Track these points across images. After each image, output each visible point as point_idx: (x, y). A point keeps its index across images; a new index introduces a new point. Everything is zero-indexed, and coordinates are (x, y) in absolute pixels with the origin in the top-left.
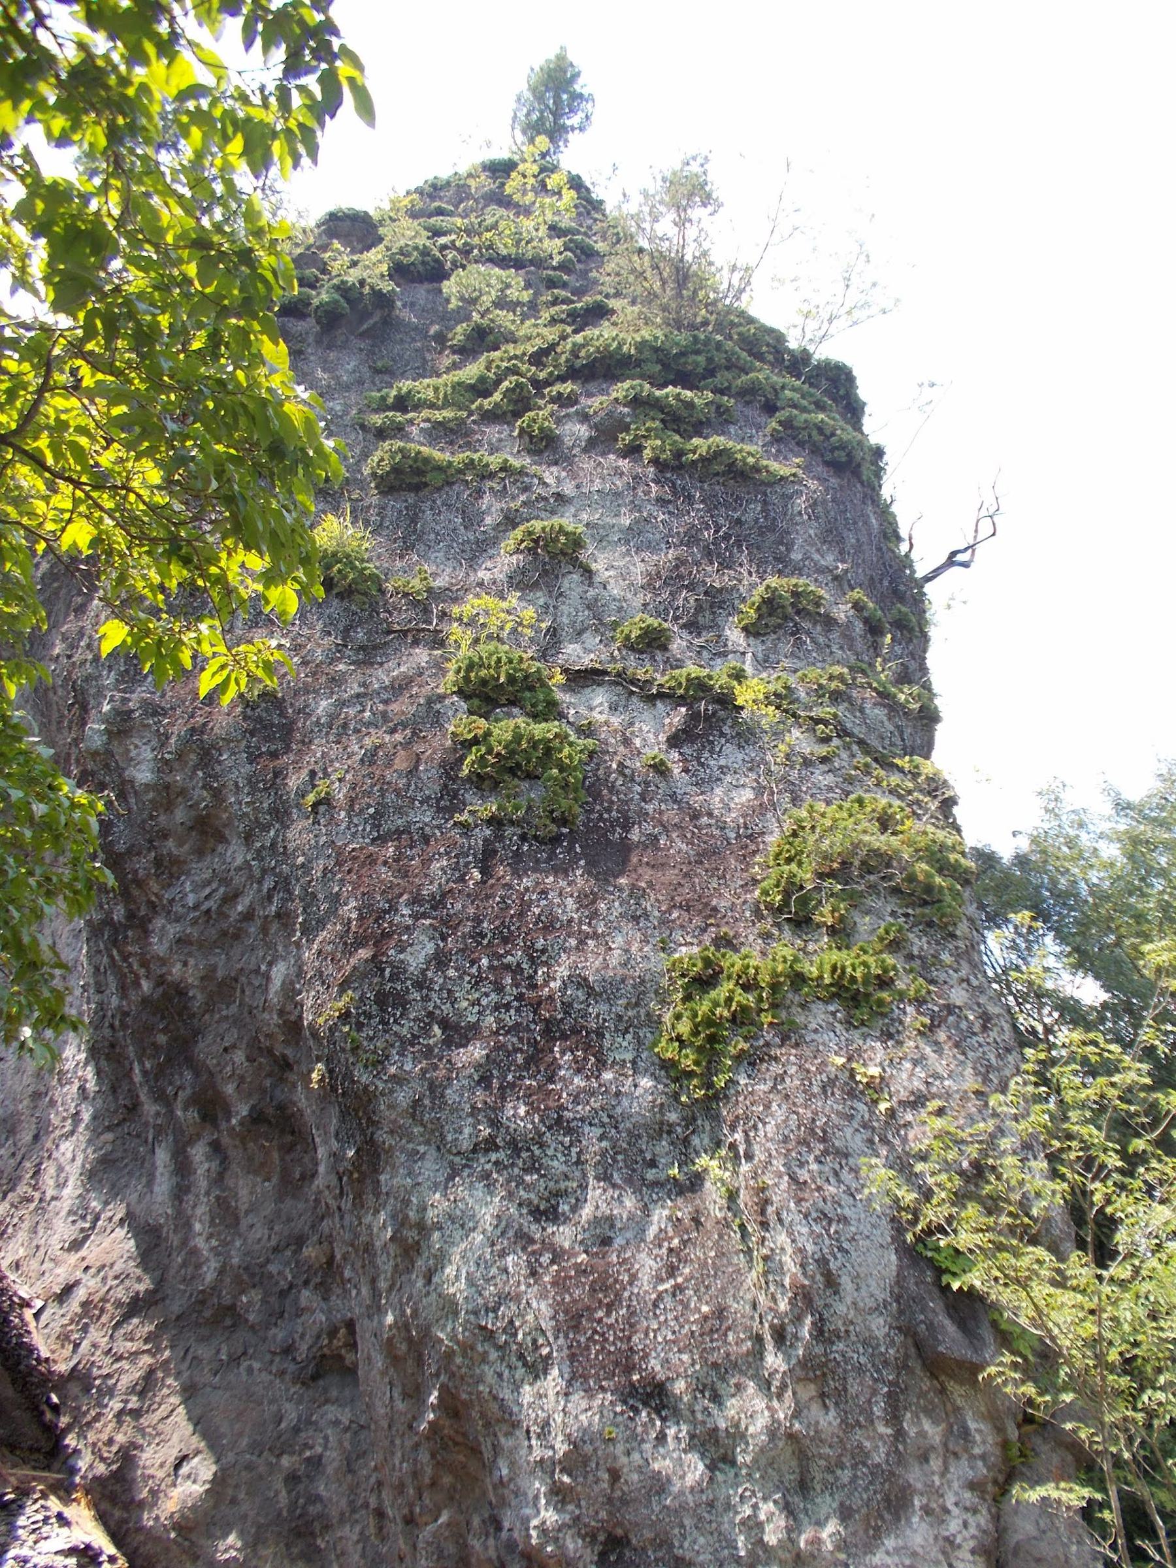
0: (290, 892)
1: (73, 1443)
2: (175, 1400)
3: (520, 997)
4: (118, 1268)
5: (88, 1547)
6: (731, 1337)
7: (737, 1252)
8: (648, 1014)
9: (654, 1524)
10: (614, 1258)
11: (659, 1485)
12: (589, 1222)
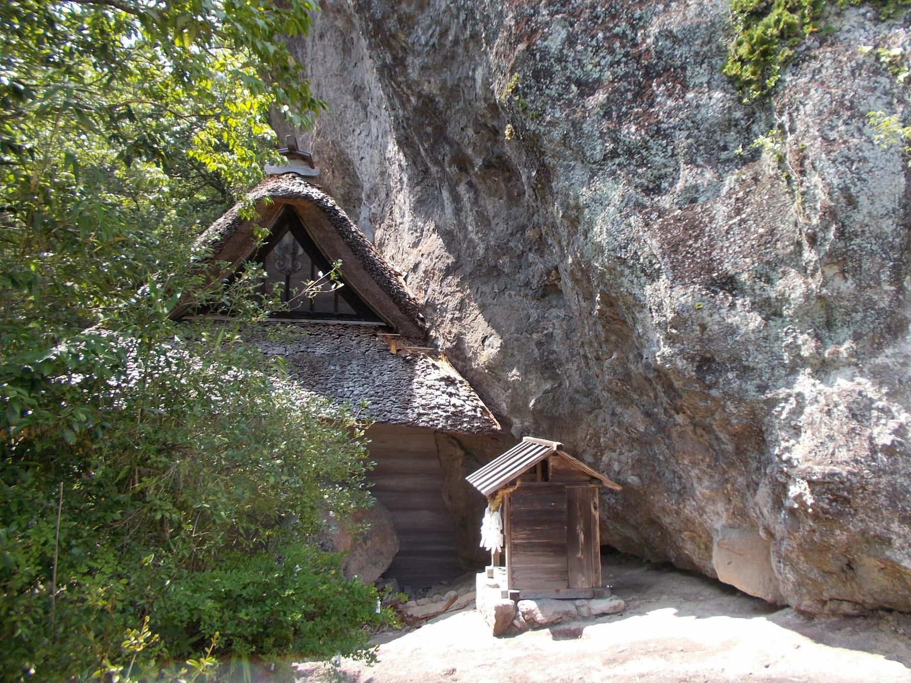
0: (474, 19)
1: (434, 334)
2: (477, 312)
3: (626, 55)
4: (437, 253)
5: (449, 377)
6: (779, 245)
7: (784, 194)
8: (718, 47)
9: (729, 350)
10: (699, 209)
11: (732, 330)
12: (681, 191)
